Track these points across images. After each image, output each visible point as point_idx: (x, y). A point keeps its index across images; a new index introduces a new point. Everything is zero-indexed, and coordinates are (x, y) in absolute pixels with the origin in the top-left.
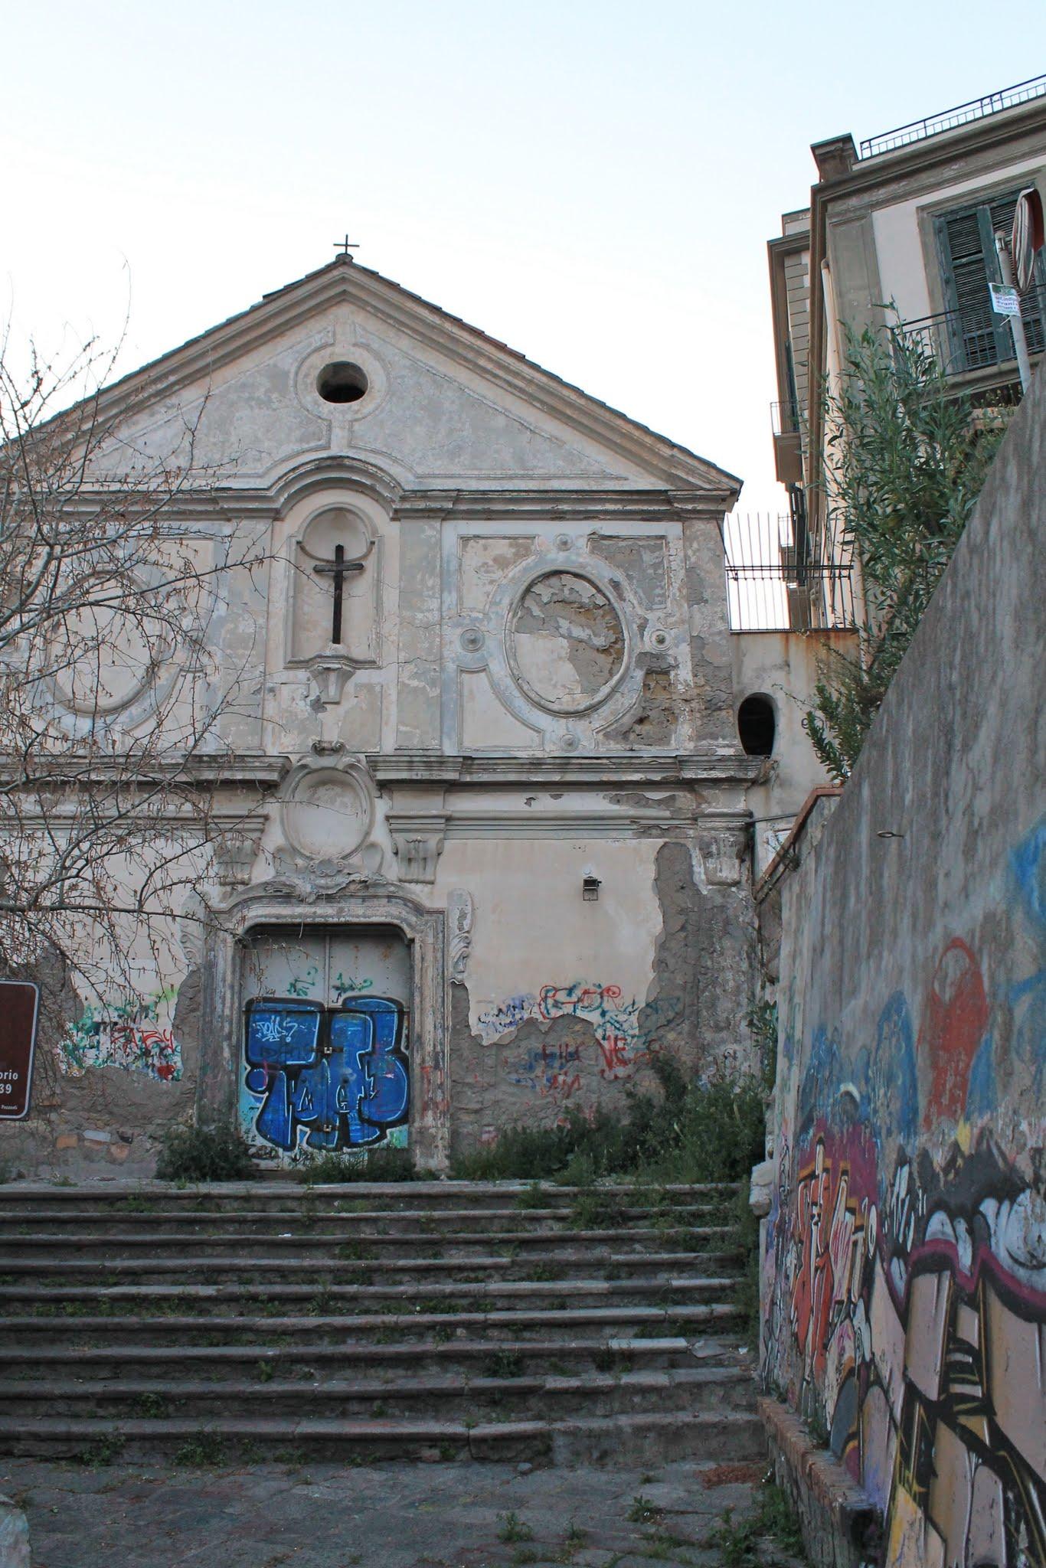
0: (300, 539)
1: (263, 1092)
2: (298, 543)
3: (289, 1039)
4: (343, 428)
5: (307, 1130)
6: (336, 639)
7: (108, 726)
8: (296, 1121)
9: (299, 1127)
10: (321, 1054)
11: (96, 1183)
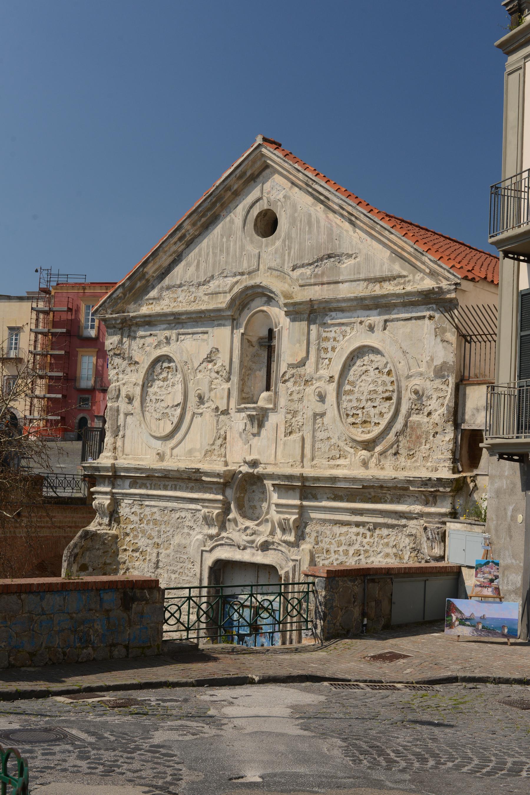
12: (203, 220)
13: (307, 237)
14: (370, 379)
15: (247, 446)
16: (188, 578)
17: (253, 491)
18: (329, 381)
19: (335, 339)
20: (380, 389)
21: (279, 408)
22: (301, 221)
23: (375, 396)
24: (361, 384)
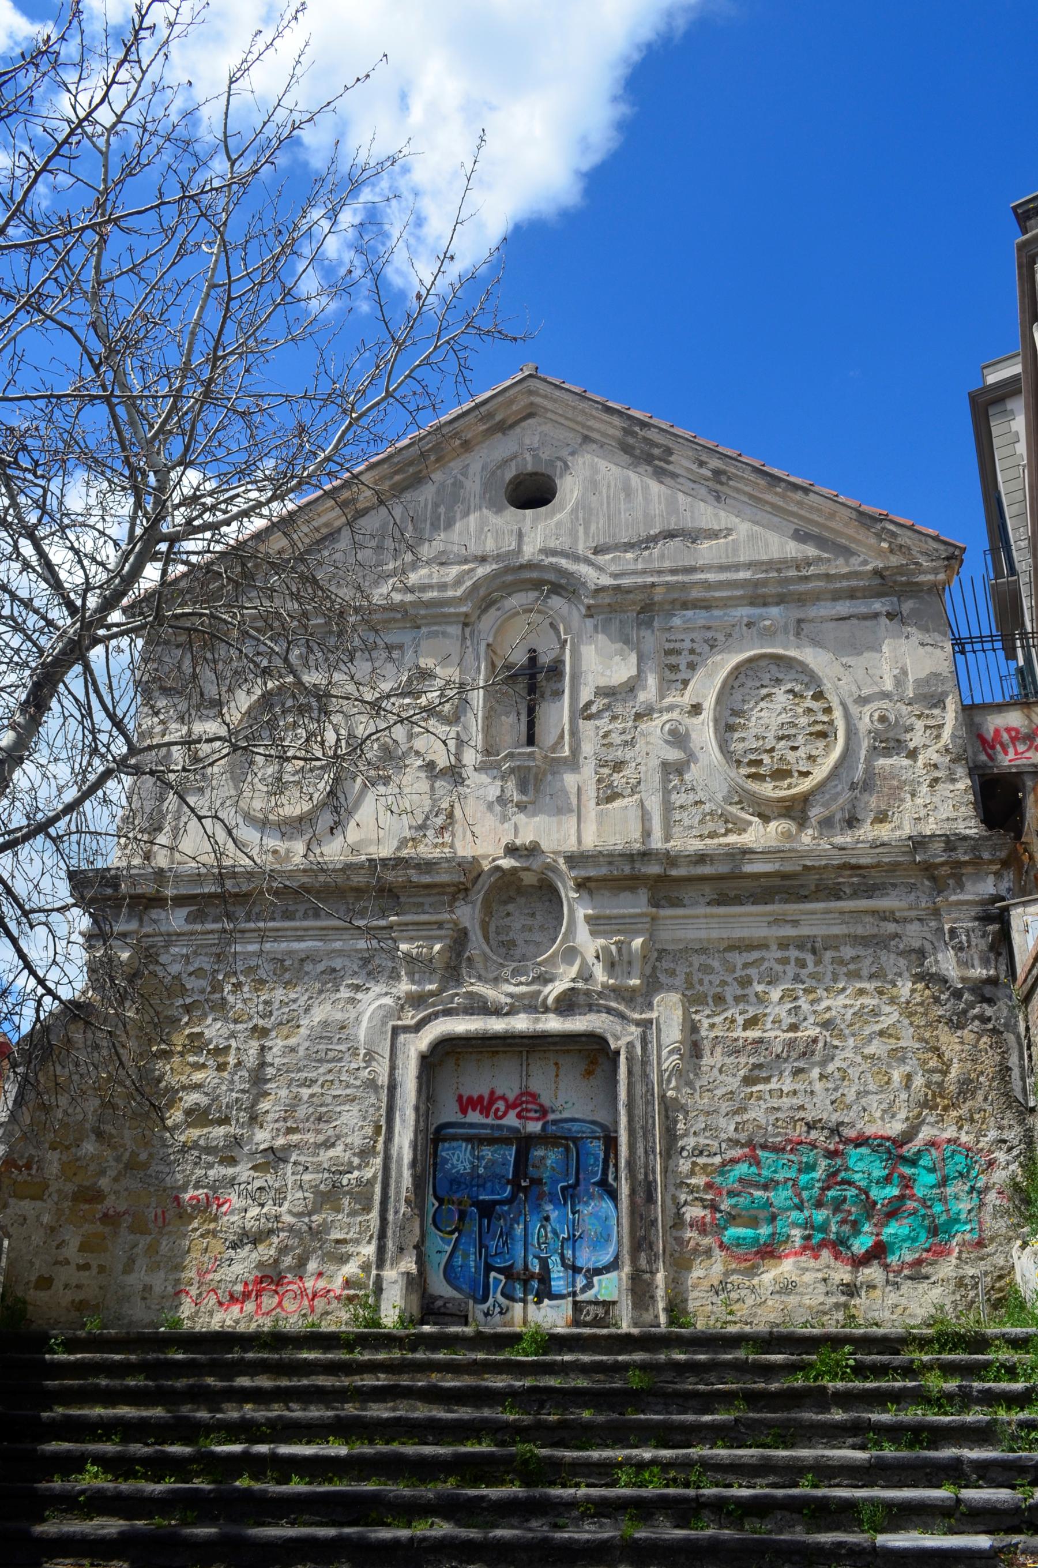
0: (490, 640)
1: (452, 1233)
2: (488, 645)
3: (481, 1171)
4: (537, 534)
5: (502, 1277)
6: (531, 741)
7: (95, 751)
8: (489, 1268)
9: (493, 1274)
10: (517, 1188)
11: (743, 528)
12: (397, 478)
13: (622, 506)
14: (779, 707)
15: (506, 825)
16: (348, 1091)
17: (508, 914)
18: (689, 712)
19: (692, 651)
20: (803, 721)
21: (581, 759)
22: (609, 487)
23: (793, 731)
24: (762, 714)
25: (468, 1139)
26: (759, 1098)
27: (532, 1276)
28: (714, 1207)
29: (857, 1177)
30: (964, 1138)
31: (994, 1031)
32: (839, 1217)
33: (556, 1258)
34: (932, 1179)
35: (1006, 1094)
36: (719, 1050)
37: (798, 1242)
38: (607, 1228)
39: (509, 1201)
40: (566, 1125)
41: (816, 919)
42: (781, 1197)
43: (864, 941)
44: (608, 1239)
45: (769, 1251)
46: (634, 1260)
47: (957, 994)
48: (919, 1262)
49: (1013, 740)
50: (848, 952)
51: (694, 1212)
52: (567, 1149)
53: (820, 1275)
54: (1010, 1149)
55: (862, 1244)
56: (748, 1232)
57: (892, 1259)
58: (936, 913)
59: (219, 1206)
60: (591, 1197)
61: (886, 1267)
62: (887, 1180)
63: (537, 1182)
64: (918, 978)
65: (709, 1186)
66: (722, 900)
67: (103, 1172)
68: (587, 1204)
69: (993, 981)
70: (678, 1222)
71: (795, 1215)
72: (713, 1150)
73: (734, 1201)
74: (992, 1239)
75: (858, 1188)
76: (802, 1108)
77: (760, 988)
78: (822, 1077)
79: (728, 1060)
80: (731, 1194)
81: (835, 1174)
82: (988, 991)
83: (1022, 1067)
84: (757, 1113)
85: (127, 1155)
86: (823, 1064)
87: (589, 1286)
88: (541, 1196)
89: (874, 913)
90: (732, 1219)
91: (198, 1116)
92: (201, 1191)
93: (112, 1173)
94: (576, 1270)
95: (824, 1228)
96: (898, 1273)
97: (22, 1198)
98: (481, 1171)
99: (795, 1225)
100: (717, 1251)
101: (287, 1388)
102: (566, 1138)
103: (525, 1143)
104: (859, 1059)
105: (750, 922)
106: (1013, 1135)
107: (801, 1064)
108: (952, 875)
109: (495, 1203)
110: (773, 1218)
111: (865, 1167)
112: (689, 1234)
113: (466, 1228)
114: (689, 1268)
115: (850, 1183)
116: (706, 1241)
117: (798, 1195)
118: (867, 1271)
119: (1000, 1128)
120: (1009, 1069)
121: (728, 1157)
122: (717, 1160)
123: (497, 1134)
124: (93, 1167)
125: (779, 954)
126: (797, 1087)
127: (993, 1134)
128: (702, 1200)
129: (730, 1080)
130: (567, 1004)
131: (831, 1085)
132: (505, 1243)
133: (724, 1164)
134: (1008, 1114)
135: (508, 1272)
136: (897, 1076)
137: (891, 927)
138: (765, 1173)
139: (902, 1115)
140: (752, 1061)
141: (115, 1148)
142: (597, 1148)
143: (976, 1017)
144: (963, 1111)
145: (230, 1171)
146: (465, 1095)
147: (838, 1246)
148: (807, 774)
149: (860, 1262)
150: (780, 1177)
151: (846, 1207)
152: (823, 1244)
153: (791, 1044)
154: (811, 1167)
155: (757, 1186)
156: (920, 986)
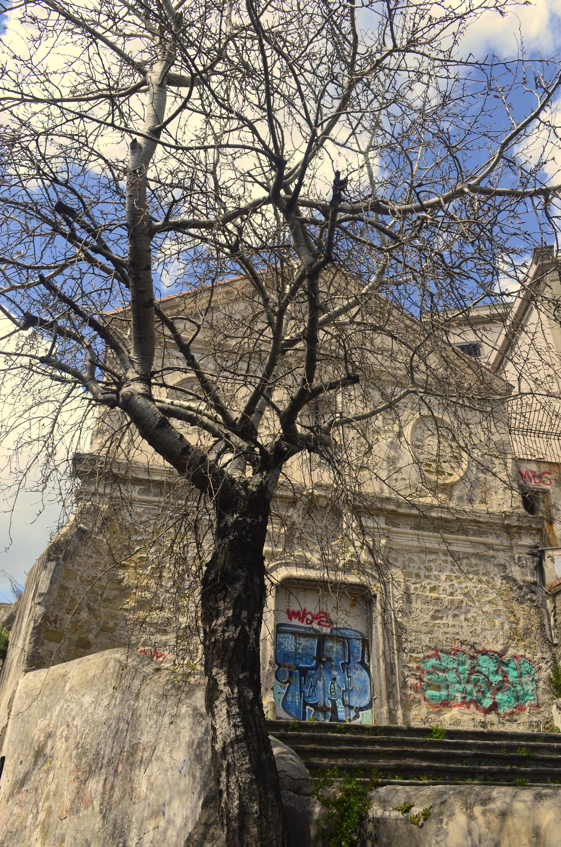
1: (285, 683)
3: (300, 651)
8: (305, 704)
9: (308, 707)
10: (319, 660)
25: (293, 633)
26: (439, 627)
27: (328, 709)
28: (421, 680)
29: (484, 670)
30: (528, 656)
31: (536, 606)
32: (477, 689)
33: (339, 701)
34: (515, 674)
35: (543, 637)
36: (419, 600)
37: (460, 700)
38: (365, 686)
39: (315, 668)
40: (343, 631)
41: (460, 544)
42: (451, 676)
43: (477, 556)
44: (366, 692)
45: (446, 703)
46: (388, 703)
47: (520, 588)
48: (512, 713)
49: (534, 476)
50: (474, 561)
51: (412, 681)
52: (344, 644)
53: (471, 717)
54: (547, 662)
55: (487, 703)
56: (436, 693)
57: (501, 711)
58: (511, 548)
59: (158, 657)
60: (357, 669)
61: (498, 714)
62: (497, 672)
63: (329, 659)
64: (504, 578)
65: (418, 668)
66: (417, 527)
67: (90, 631)
68: (355, 673)
69: (535, 583)
70: (404, 685)
71: (458, 686)
72: (420, 650)
73: (430, 677)
74: (543, 704)
75: (485, 675)
76: (458, 633)
77: (436, 573)
78: (466, 619)
79: (425, 606)
80: (429, 673)
81: (474, 668)
82: (533, 588)
83: (550, 625)
84: (439, 634)
85: (102, 622)
86: (466, 613)
87: (357, 716)
88: (331, 667)
89: (485, 544)
90: (429, 686)
91: (142, 604)
92: (147, 648)
93: (95, 632)
94: (351, 708)
95: (471, 694)
96: (504, 718)
97: (51, 640)
98: (300, 651)
99: (457, 691)
100: (423, 702)
101: (346, 750)
102: (343, 638)
103: (322, 639)
104: (481, 613)
105: (431, 540)
106: (547, 656)
107: (456, 612)
108: (517, 533)
109: (308, 669)
110: (447, 687)
111: (487, 665)
112: (409, 692)
113: (293, 681)
114: (410, 710)
115: (481, 672)
116: (418, 696)
117: (459, 676)
118: (490, 716)
119: (542, 652)
120: (544, 625)
121: (426, 654)
122: (421, 655)
123: (308, 632)
124: (85, 627)
125: (443, 558)
126: (455, 623)
127: (539, 655)
128: (415, 675)
129: (425, 616)
130: (348, 568)
131: (470, 624)
132: (313, 691)
133: (424, 658)
134: (545, 646)
135: (314, 706)
136: (497, 622)
137: (492, 553)
138: (443, 664)
139: (501, 641)
140: (435, 608)
141: (96, 618)
142: (358, 644)
143: (529, 599)
144: (526, 643)
145: (164, 638)
146: (291, 609)
147: (477, 703)
148: (451, 475)
149: (487, 711)
150: (450, 666)
151: (479, 684)
152: (471, 701)
153: (452, 602)
154: (464, 663)
155: (440, 670)
156: (504, 582)
